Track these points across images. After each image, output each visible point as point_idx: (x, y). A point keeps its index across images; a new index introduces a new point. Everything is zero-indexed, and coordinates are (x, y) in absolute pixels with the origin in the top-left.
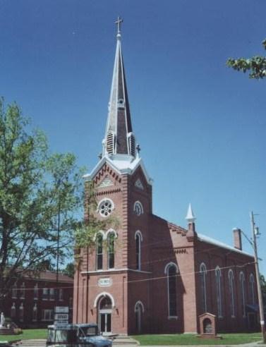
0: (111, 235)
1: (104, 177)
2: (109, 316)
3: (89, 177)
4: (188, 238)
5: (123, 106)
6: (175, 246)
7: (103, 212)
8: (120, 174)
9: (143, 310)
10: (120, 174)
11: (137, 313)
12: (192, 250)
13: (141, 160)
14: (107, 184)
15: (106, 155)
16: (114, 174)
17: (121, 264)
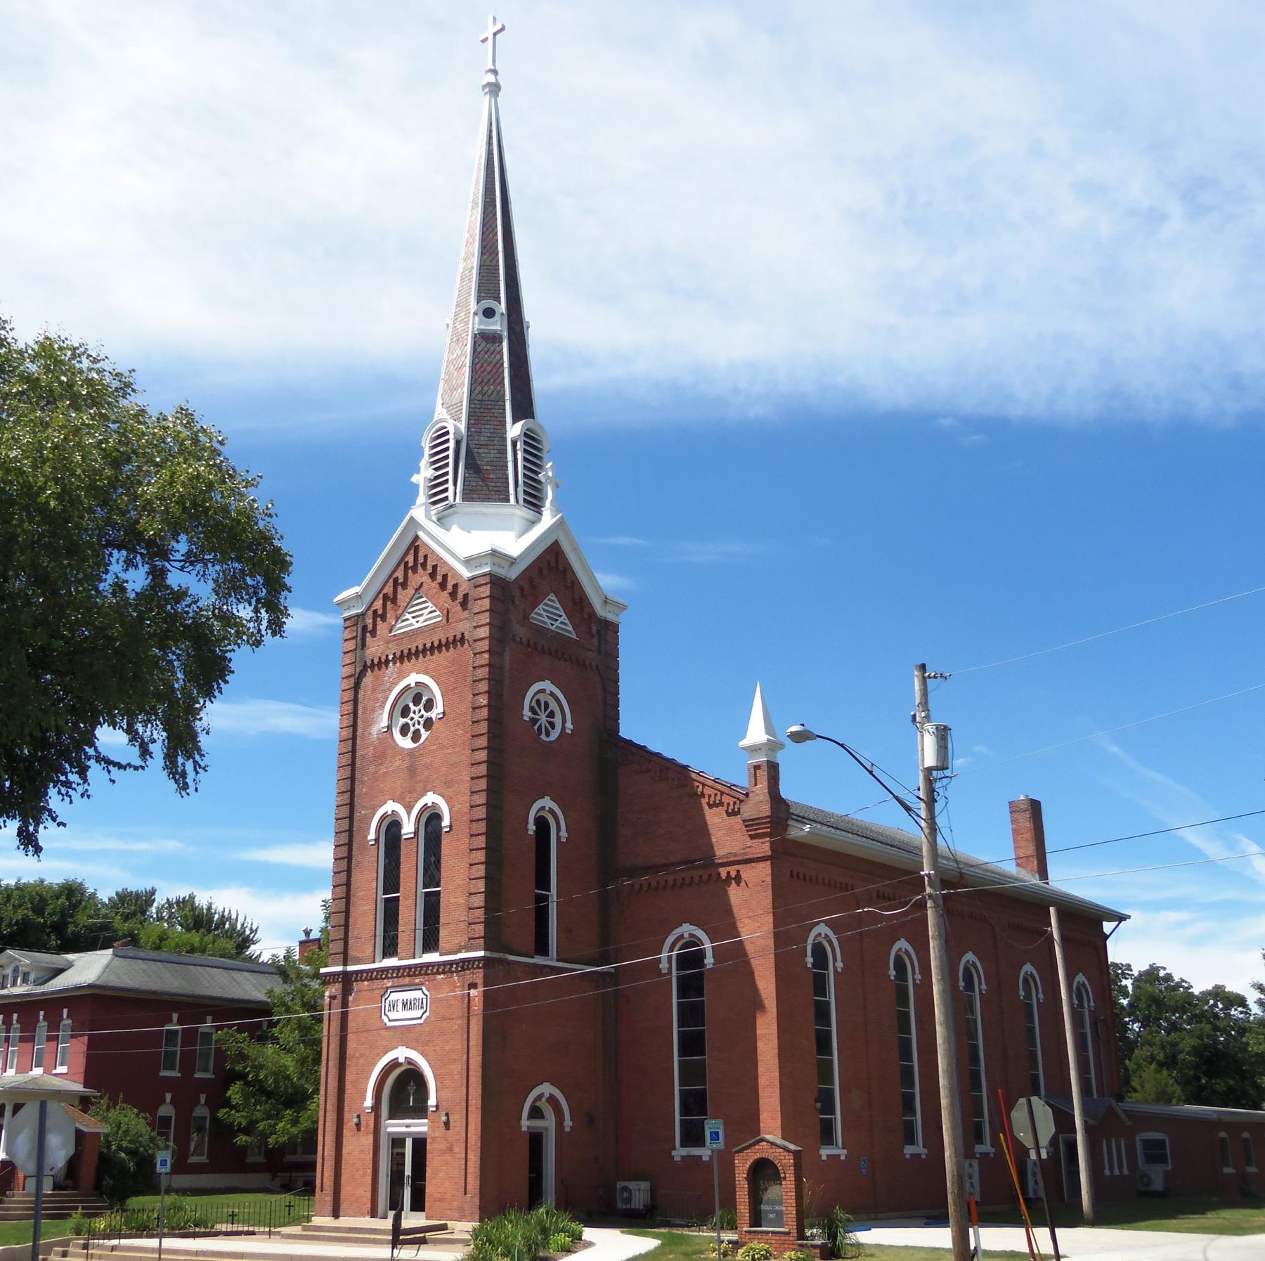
0: (431, 819)
1: (410, 591)
2: (420, 1144)
3: (358, 597)
4: (749, 824)
5: (498, 325)
6: (719, 852)
7: (404, 730)
8: (466, 573)
9: (568, 1123)
10: (466, 573)
11: (536, 1140)
12: (764, 869)
13: (560, 525)
14: (421, 616)
15: (419, 511)
16: (455, 586)
17: (462, 943)
